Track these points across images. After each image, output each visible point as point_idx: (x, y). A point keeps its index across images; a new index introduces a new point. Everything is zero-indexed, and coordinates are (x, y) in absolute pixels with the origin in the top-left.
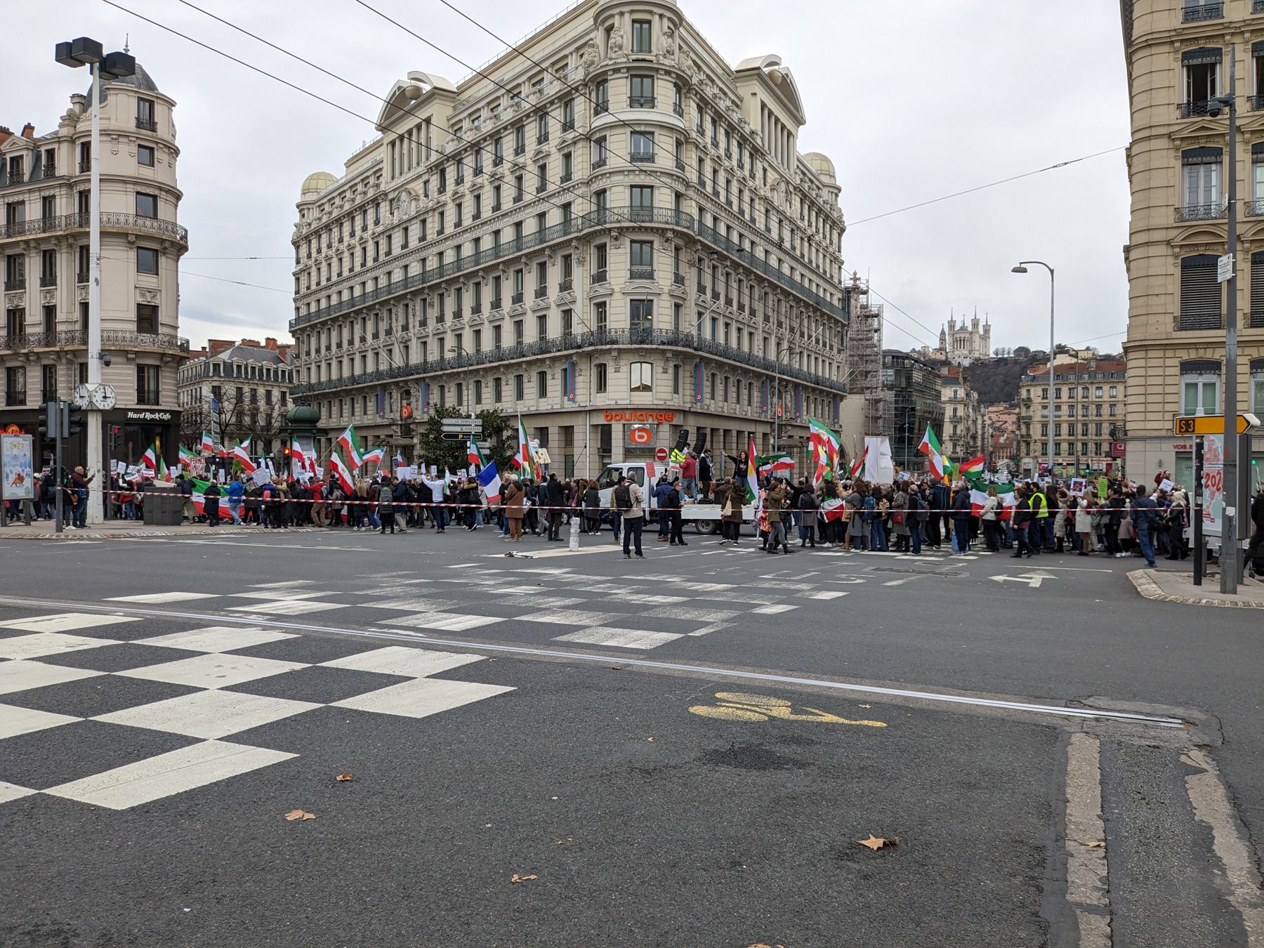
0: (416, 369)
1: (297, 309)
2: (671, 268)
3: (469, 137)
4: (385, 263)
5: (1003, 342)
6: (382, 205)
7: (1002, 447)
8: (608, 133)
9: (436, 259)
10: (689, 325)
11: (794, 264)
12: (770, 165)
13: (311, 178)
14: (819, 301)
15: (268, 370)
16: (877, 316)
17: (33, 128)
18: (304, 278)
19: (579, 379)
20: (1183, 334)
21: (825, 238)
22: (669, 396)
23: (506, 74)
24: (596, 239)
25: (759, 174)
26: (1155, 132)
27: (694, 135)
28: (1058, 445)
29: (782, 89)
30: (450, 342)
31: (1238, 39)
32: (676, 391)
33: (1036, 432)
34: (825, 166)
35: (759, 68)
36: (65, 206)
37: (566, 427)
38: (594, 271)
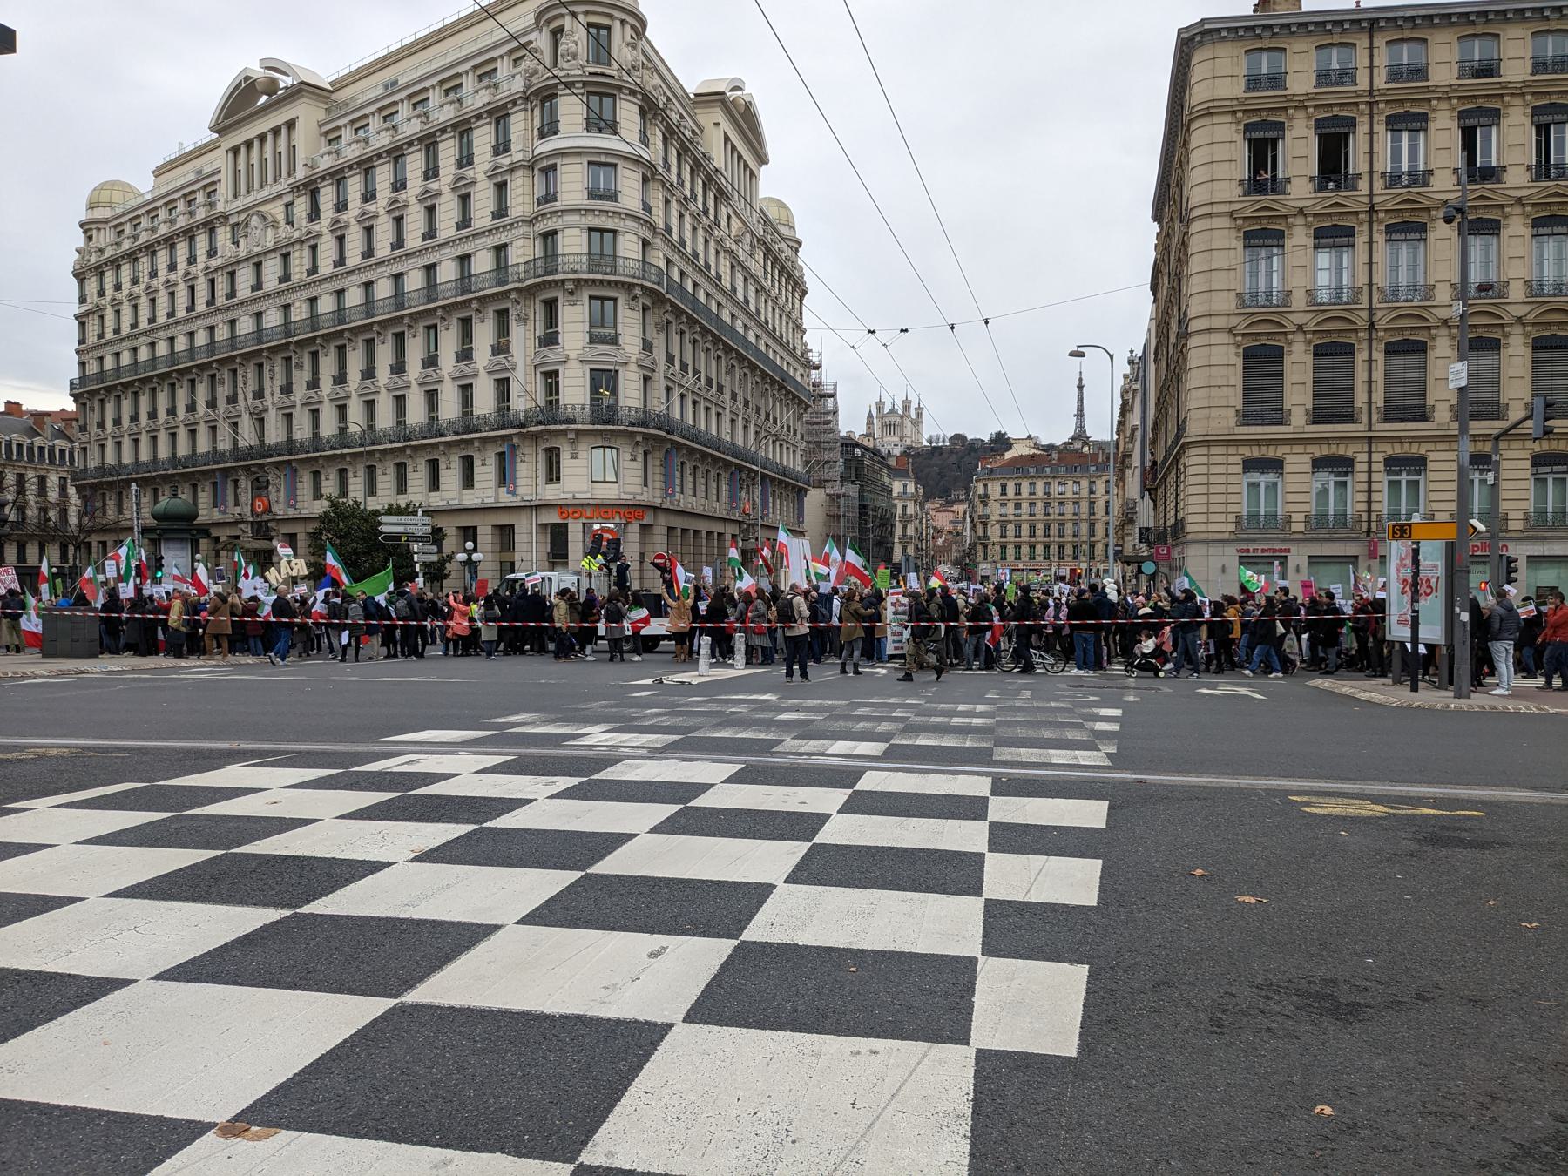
0: (277, 450)
1: (82, 364)
2: (638, 332)
5: (936, 428)
6: (220, 231)
7: (940, 550)
8: (559, 162)
9: (305, 307)
10: (658, 405)
12: (735, 212)
13: (101, 187)
14: (785, 376)
15: (20, 446)
16: (832, 396)
19: (521, 467)
20: (1245, 429)
22: (638, 489)
23: (406, 73)
24: (545, 294)
26: (1216, 209)
28: (1061, 547)
29: (745, 120)
30: (356, 413)
31: (1301, 114)
32: (646, 485)
33: (994, 533)
34: (783, 216)
35: (723, 93)
37: (502, 527)
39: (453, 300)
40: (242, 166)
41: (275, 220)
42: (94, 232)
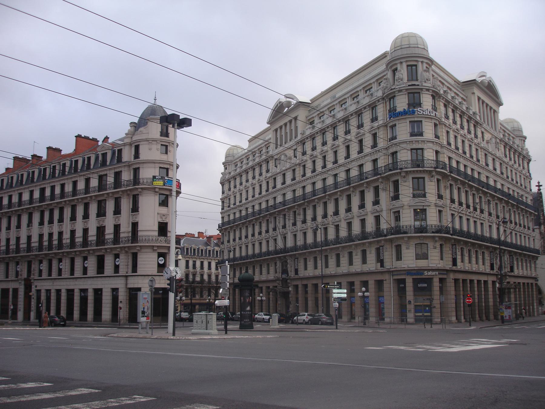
1: (223, 218)
3: (319, 126)
4: (272, 193)
6: (270, 162)
9: (301, 190)
10: (447, 221)
11: (503, 183)
15: (202, 250)
17: (108, 138)
18: (227, 201)
21: (519, 165)
22: (437, 262)
23: (339, 93)
25: (480, 135)
27: (443, 120)
29: (490, 89)
32: (442, 259)
35: (475, 80)
36: (127, 176)
38: (392, 194)
39: (357, 184)
40: (278, 136)
41: (289, 156)
42: (228, 166)
